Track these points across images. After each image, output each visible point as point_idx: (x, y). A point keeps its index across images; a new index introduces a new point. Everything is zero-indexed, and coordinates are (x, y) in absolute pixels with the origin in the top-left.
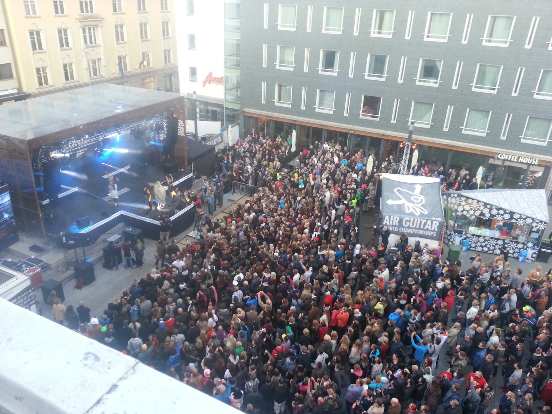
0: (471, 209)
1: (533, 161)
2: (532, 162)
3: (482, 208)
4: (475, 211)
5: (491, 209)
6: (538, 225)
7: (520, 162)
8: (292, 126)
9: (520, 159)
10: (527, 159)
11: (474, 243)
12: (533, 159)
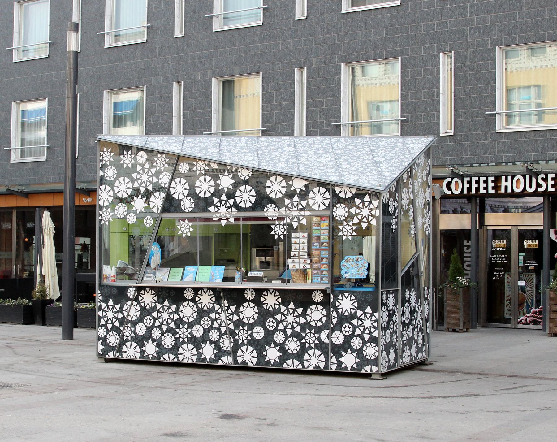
0: (137, 192)
1: (541, 182)
2: (538, 185)
3: (165, 179)
4: (148, 195)
5: (191, 177)
6: (353, 210)
7: (506, 195)
8: (12, 208)
9: (503, 184)
10: (521, 178)
11: (170, 330)
12: (537, 174)
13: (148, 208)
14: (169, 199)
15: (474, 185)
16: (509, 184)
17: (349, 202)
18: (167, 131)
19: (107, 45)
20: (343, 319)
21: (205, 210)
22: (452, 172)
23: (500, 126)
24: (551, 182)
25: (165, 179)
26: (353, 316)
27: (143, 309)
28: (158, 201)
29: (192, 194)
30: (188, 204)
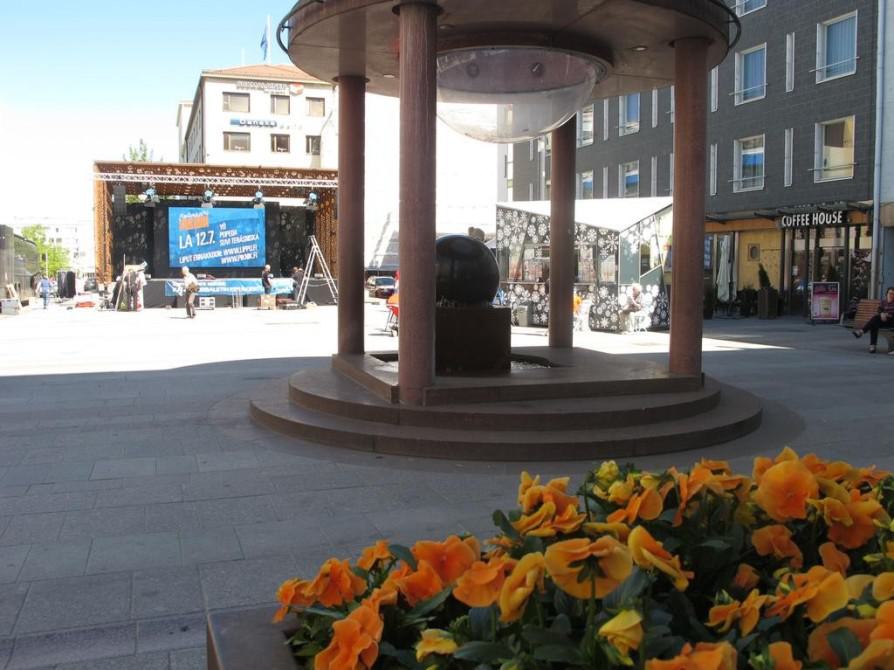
2: (833, 219)
13: (518, 242)
14: (527, 235)
15: (798, 220)
16: (816, 219)
17: (605, 237)
18: (506, 200)
19: (736, 104)
20: (603, 301)
21: (542, 242)
22: (755, 214)
23: (816, 180)
24: (840, 217)
25: (525, 226)
26: (606, 299)
27: (541, 296)
28: (522, 237)
29: (537, 233)
30: (535, 239)
